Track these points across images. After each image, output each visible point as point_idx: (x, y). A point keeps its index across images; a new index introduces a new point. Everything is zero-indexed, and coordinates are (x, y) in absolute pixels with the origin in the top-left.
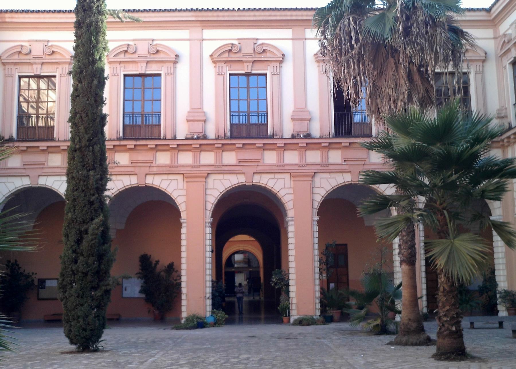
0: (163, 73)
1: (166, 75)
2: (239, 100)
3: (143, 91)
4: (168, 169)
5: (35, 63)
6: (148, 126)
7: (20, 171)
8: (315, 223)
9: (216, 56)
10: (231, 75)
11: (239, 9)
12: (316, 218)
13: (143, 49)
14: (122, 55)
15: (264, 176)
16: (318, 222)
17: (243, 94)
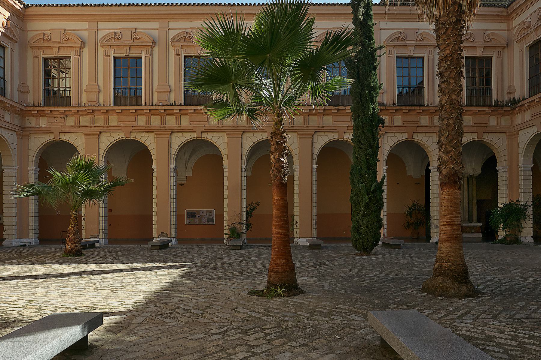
0: (72, 56)
1: (146, 56)
2: (416, 77)
3: (409, 70)
4: (144, 128)
5: (409, 46)
6: (344, 96)
7: (115, 128)
8: (314, 170)
9: (389, 41)
10: (398, 57)
11: (61, 5)
12: (315, 166)
13: (127, 36)
14: (396, 41)
15: (419, 134)
16: (317, 169)
17: (406, 73)
